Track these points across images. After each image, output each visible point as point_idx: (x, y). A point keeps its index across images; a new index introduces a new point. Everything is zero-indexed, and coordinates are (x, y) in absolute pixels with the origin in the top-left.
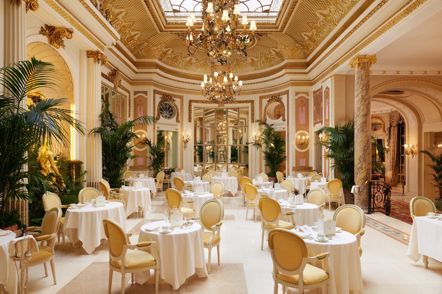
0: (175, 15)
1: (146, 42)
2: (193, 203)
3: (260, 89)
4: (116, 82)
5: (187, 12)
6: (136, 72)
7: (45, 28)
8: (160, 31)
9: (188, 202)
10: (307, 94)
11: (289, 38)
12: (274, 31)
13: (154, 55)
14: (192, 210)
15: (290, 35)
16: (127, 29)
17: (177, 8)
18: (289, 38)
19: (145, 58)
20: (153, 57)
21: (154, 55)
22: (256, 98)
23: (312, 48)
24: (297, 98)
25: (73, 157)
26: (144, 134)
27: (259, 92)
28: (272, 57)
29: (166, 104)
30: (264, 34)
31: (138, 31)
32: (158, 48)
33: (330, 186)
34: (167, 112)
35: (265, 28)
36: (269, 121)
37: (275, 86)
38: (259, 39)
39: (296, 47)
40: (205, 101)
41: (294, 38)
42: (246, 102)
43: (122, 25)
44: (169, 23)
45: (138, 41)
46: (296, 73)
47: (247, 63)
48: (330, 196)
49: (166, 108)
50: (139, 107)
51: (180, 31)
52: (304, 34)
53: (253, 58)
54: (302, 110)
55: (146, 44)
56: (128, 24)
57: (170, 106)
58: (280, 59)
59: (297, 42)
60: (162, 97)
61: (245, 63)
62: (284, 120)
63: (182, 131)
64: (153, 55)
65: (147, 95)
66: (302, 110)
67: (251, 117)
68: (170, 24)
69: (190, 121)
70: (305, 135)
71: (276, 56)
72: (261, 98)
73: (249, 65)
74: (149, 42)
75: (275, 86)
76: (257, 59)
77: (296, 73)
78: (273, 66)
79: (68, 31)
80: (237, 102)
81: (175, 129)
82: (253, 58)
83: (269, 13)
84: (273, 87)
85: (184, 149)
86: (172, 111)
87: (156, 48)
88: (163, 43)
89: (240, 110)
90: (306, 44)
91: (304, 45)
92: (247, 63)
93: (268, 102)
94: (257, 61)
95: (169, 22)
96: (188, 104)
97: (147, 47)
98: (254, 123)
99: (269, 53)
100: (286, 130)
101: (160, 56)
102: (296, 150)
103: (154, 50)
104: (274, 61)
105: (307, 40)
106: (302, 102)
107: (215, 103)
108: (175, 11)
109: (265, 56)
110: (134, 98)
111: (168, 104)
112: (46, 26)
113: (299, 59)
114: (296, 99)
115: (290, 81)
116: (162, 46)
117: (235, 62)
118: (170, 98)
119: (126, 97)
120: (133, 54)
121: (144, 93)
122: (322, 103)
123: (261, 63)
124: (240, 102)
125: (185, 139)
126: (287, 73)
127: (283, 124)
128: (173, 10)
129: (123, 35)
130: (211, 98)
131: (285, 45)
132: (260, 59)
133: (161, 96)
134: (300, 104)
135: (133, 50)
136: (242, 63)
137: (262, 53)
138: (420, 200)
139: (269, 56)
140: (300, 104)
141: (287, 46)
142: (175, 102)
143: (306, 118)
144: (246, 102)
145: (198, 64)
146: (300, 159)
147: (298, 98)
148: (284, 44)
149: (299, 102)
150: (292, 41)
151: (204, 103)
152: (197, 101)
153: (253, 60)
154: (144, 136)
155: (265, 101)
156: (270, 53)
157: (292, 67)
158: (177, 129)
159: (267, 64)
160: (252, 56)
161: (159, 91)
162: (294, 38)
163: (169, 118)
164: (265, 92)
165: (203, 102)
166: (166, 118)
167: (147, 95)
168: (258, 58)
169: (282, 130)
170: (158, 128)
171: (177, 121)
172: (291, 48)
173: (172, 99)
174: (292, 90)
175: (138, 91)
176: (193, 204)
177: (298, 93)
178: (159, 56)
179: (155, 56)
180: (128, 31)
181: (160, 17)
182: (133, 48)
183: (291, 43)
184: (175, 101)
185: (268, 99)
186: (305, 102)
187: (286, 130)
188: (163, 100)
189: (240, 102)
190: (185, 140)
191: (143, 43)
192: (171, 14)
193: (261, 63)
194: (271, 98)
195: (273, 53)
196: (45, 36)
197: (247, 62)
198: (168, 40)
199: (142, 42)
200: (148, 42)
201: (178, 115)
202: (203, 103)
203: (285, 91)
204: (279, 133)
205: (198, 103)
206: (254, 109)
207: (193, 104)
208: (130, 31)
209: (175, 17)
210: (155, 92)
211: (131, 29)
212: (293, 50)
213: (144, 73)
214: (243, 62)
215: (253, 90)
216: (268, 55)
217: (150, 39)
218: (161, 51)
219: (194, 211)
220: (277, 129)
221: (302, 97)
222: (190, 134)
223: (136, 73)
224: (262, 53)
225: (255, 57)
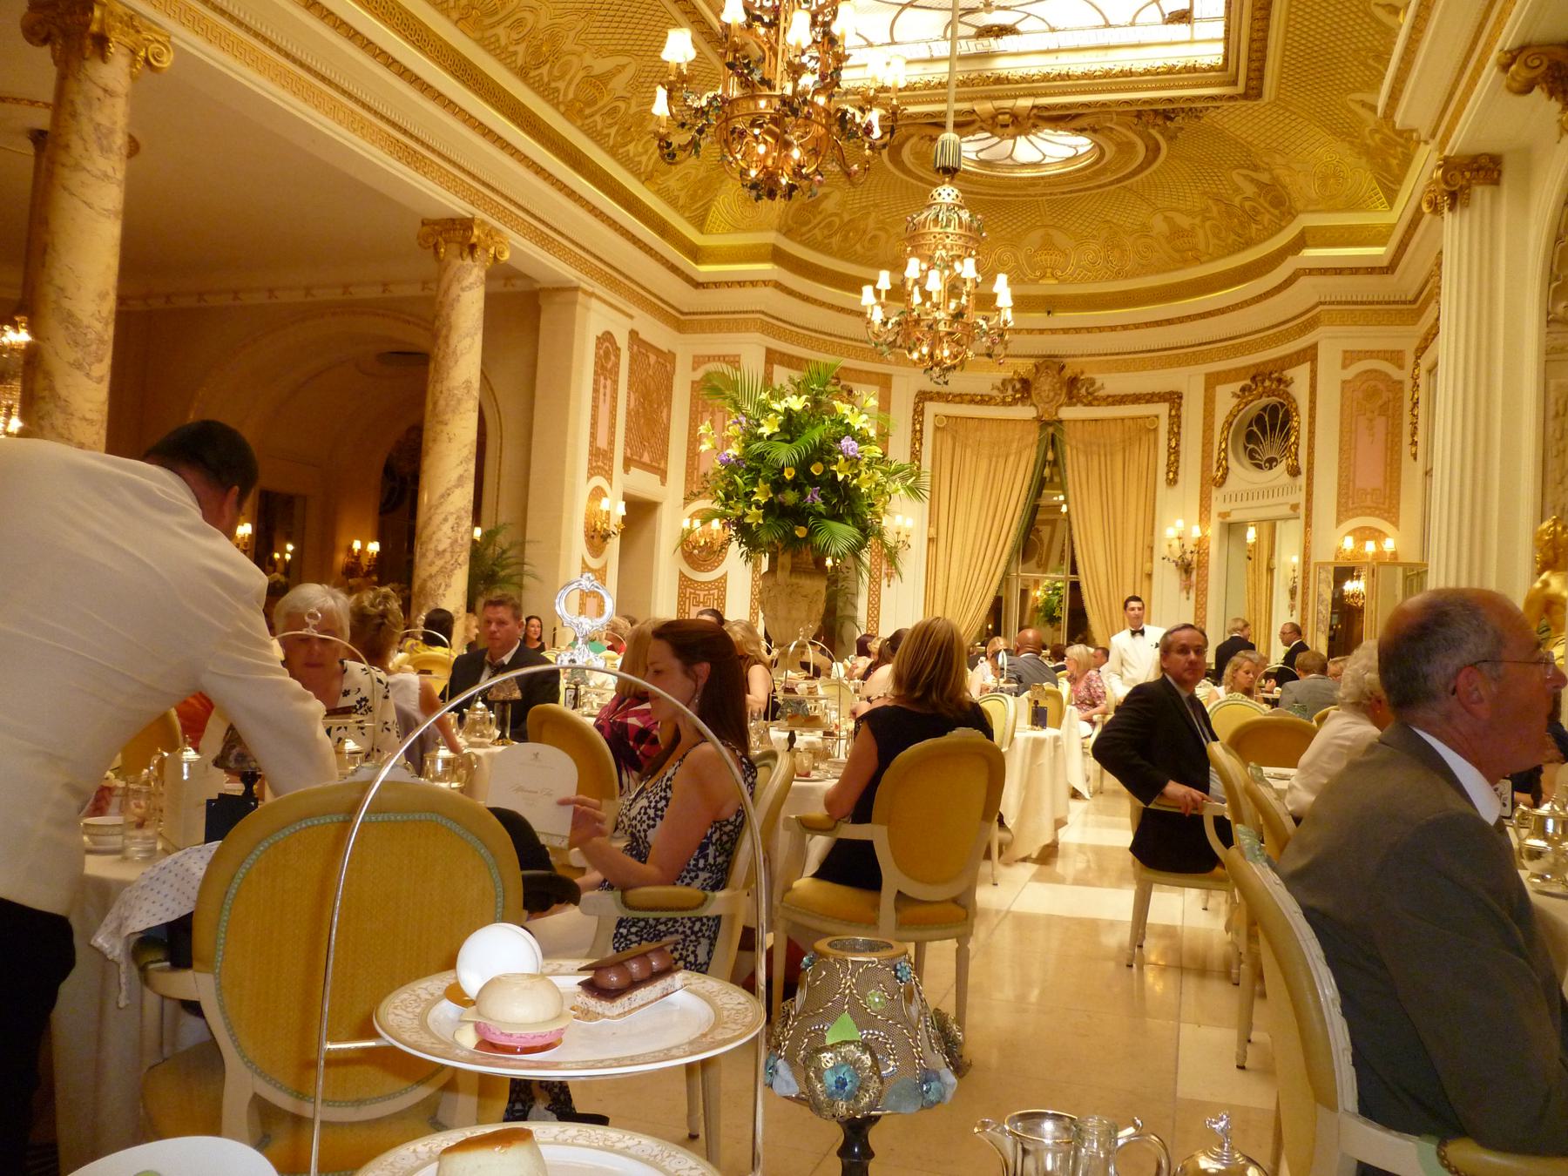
5: (1053, 30)
22: (1190, 381)
38: (1171, 138)
42: (1151, 398)
52: (1357, 102)
58: (1277, 212)
62: (1294, 472)
70: (1378, 535)
72: (1213, 381)
83: (1197, 25)
93: (1235, 401)
106: (1372, 394)
115: (1321, 303)
122: (665, 411)
124: (1122, 400)
144: (1151, 398)
161: (791, 357)
185: (1236, 387)
189: (1122, 400)
194: (1248, 382)
195: (1250, 190)
203: (1304, 350)
206: (1179, 427)
207: (932, 408)
210: (772, 357)
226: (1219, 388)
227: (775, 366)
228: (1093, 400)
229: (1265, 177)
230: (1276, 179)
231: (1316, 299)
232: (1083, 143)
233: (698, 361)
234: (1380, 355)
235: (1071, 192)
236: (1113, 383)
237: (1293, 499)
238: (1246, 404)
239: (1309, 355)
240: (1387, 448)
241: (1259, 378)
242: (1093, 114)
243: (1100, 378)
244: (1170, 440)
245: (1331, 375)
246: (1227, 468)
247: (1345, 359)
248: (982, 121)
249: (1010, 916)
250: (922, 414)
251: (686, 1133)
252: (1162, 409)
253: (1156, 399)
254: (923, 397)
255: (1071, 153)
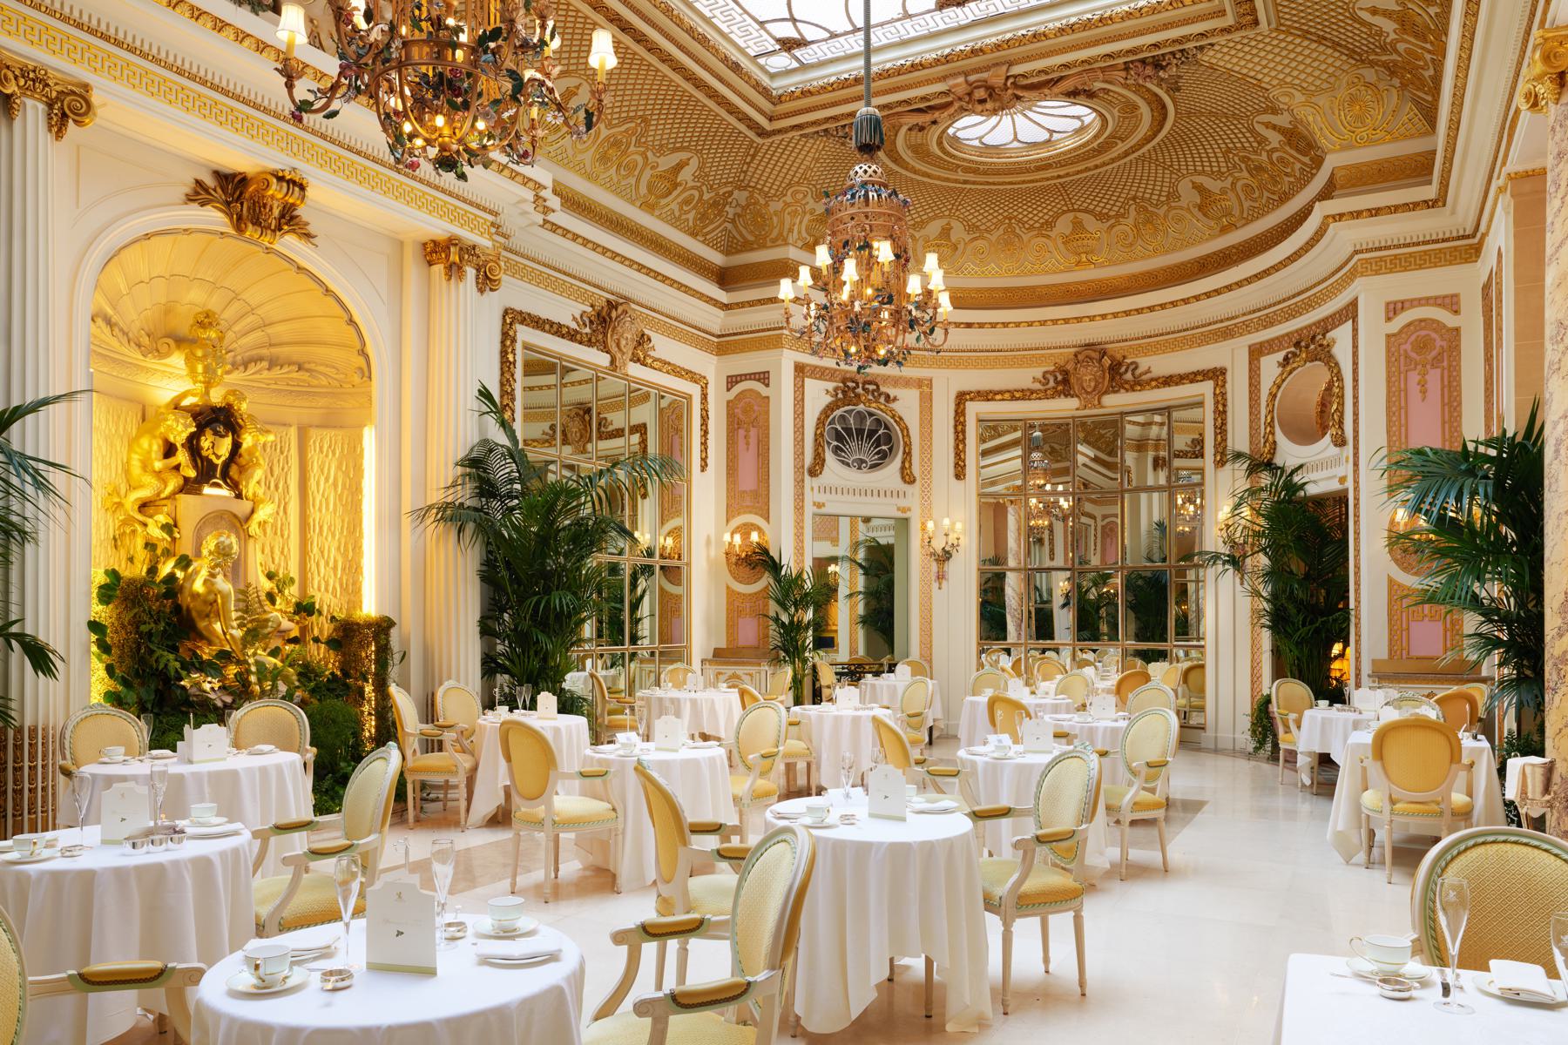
0: (797, 60)
1: (739, 188)
2: (609, 777)
3: (1250, 313)
4: (618, 345)
5: (834, 36)
6: (726, 305)
7: (210, 182)
8: (759, 135)
9: (583, 775)
10: (1451, 303)
11: (1315, 50)
12: (1213, 32)
13: (780, 234)
14: (605, 806)
15: (1311, 33)
16: (632, 148)
17: (787, 31)
18: (1315, 50)
19: (752, 250)
20: (780, 242)
21: (780, 234)
22: (1231, 355)
23: (1431, 72)
24: (1395, 331)
25: (369, 608)
26: (759, 529)
27: (1246, 328)
28: (1275, 156)
29: (861, 417)
30: (1173, 54)
31: (682, 149)
32: (787, 205)
33: (1387, 753)
34: (866, 446)
35: (1167, 26)
36: (1289, 453)
37: (1307, 290)
39: (1368, 85)
40: (1023, 391)
41: (1334, 42)
43: (602, 137)
44: (780, 96)
45: (704, 188)
46: (1375, 212)
47: (1182, 208)
48: (1393, 802)
49: (860, 432)
50: (741, 432)
51: (827, 120)
53: (1199, 179)
54: (1423, 384)
55: (741, 196)
56: (623, 128)
57: (878, 421)
58: (1306, 160)
59: (1363, 61)
60: (836, 389)
61: (1175, 208)
63: (927, 514)
64: (774, 234)
65: (767, 385)
66: (1423, 384)
67: (1215, 440)
68: (783, 99)
69: (960, 474)
71: (1288, 148)
72: (1256, 352)
73: (1194, 216)
74: (748, 186)
75: (1307, 290)
76: (1219, 184)
77: (1375, 212)
78: (1288, 199)
79: (280, 179)
80: (1154, 383)
81: (899, 509)
82: (1199, 179)
84: (1299, 294)
85: (935, 585)
86: (888, 439)
87: (781, 204)
88: (796, 179)
89: (1176, 415)
90: (1400, 55)
91: (1395, 63)
92: (1182, 208)
94: (1223, 191)
95: (781, 92)
96: (952, 407)
97: (748, 205)
98: (1228, 466)
99: (1255, 145)
100: (1350, 484)
101: (804, 234)
102: (1391, 581)
103: (776, 213)
104: (1287, 174)
105: (1393, 36)
106: (1423, 346)
107: (1066, 396)
108: (788, 45)
109: (1245, 159)
110: (728, 402)
111: (871, 415)
112: (217, 174)
113: (1395, 139)
114: (1388, 336)
115: (1356, 252)
116: (797, 192)
117: (1133, 213)
118: (874, 391)
119: (689, 398)
120: (703, 242)
121: (759, 380)
123: (1238, 195)
124: (1168, 381)
125: (938, 545)
126: (1333, 217)
127: (1336, 462)
128: (778, 41)
129: (623, 172)
130: (1048, 376)
131: (1305, 85)
132: (1230, 179)
133: (831, 386)
134: (1413, 355)
135: (695, 226)
136: (1161, 212)
137: (1229, 150)
138: (1481, 850)
139: (1264, 156)
140: (1413, 355)
141: (1320, 90)
142: (893, 405)
143: (1444, 423)
145: (979, 243)
146: (1413, 625)
147: (1401, 331)
148: (1297, 82)
149: (1408, 347)
150: (1331, 59)
151: (1018, 399)
152: (987, 396)
153: (1205, 189)
154: (755, 537)
155: (1270, 366)
156: (1262, 141)
157: (1365, 184)
158: (904, 510)
159: (1266, 194)
160: (1192, 174)
162: (1336, 45)
163: (873, 466)
164: (1269, 322)
165: (1014, 395)
166: (859, 468)
167: (767, 385)
168: (1220, 175)
169: (1334, 486)
170: (819, 505)
171: (903, 478)
172: (1343, 93)
173: (880, 395)
174: (1371, 293)
175: (736, 376)
176: (605, 783)
177: (1399, 305)
178: (799, 232)
179: (785, 234)
180: (639, 159)
181: (721, 80)
182: (691, 216)
183: (1331, 70)
184: (895, 399)
185: (1280, 356)
186: (1439, 343)
187: (1350, 484)
188: (838, 400)
189: (1168, 381)
190: (939, 551)
191: (731, 193)
192: (781, 61)
193: (1238, 195)
194: (1293, 349)
196: (209, 207)
197: (1184, 202)
198: (808, 168)
199: (721, 192)
200: (745, 188)
201: (908, 454)
202: (1013, 398)
204: (1319, 501)
205: (993, 399)
207: (974, 409)
208: (649, 154)
209: (804, 67)
211: (647, 149)
212: (1353, 100)
213: (751, 304)
214: (1165, 207)
215: (1222, 321)
216: (1255, 152)
217: (745, 172)
218: (804, 213)
219: (614, 810)
220: (1318, 484)
221: (1421, 321)
222: (959, 526)
223: (726, 307)
224: (1229, 150)
225: (1208, 175)
226: (1263, 360)
227: (807, 381)
228: (1138, 384)
229: (1283, 120)
230: (1296, 121)
231: (1351, 249)
232: (1083, 112)
233: (732, 381)
234: (1432, 301)
235: (1078, 172)
236: (1161, 364)
237: (1340, 471)
238: (1290, 373)
239: (1350, 312)
240: (1443, 405)
241: (1303, 344)
242: (1073, 75)
243: (1144, 363)
244: (1215, 419)
245: (1373, 329)
246: (1275, 442)
247: (1387, 312)
248: (960, 99)
249: (158, 996)
250: (964, 415)
251: (924, 1013)
252: (1206, 388)
253: (1199, 378)
254: (962, 398)
255: (1077, 124)
